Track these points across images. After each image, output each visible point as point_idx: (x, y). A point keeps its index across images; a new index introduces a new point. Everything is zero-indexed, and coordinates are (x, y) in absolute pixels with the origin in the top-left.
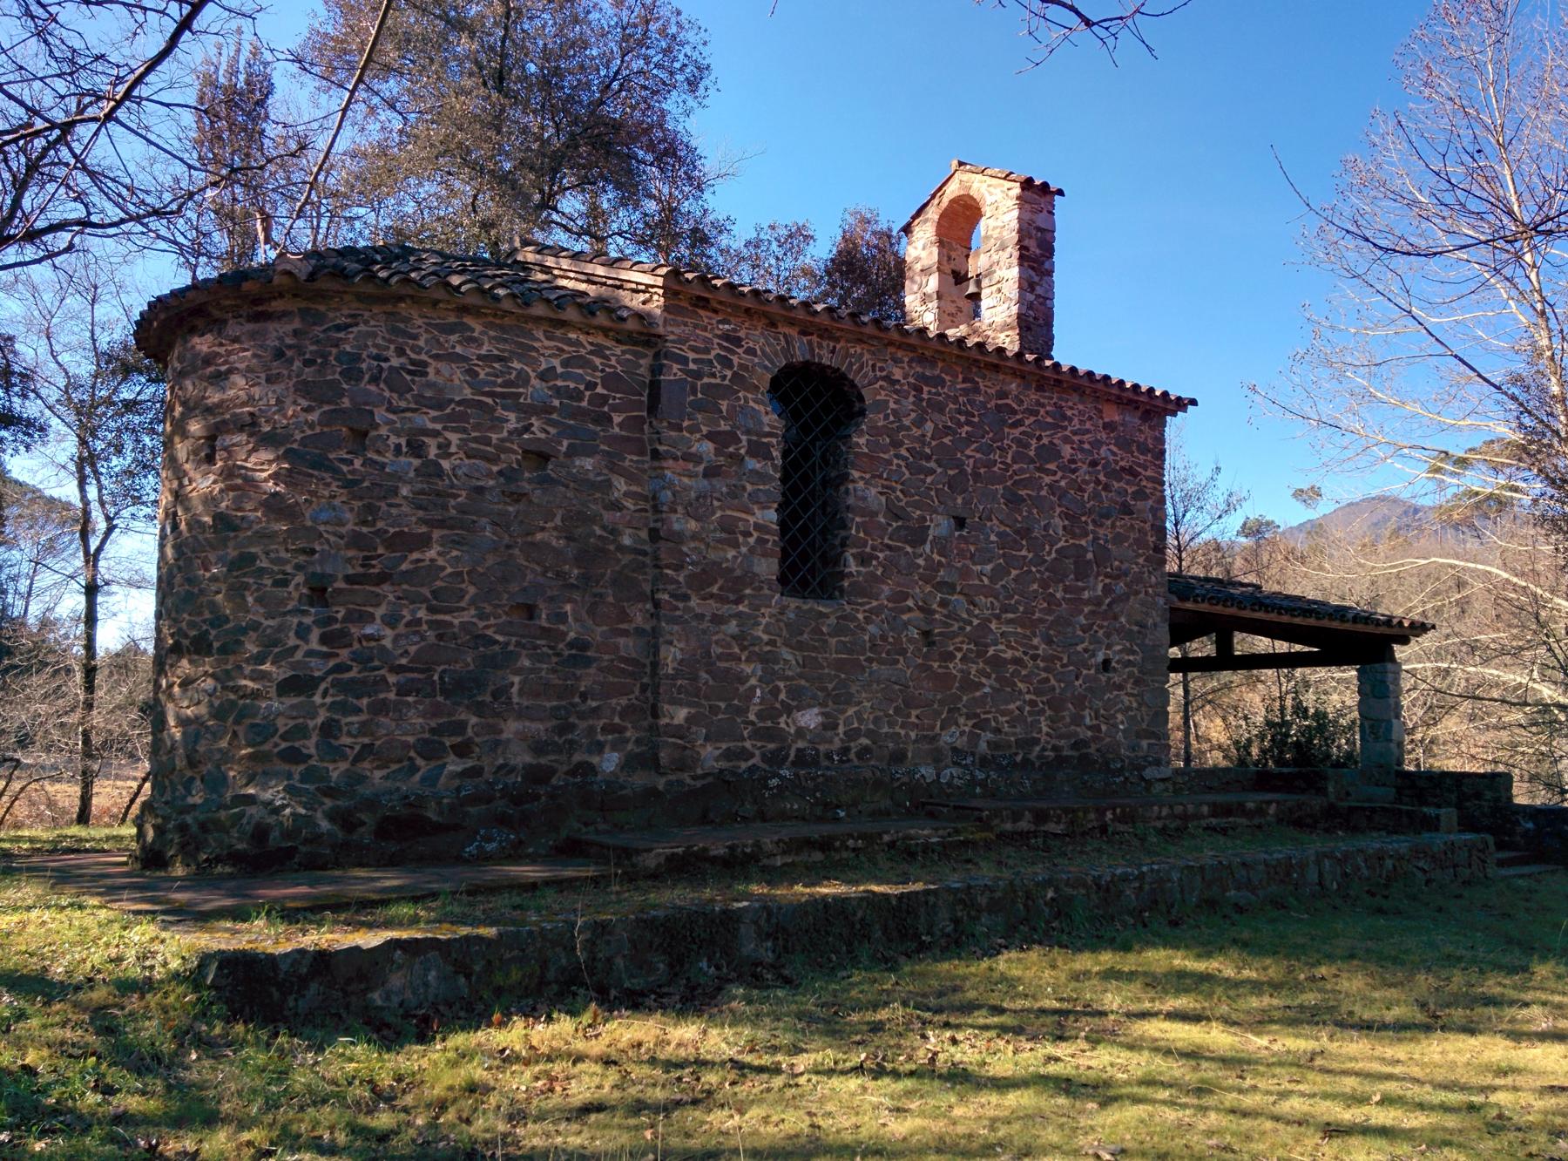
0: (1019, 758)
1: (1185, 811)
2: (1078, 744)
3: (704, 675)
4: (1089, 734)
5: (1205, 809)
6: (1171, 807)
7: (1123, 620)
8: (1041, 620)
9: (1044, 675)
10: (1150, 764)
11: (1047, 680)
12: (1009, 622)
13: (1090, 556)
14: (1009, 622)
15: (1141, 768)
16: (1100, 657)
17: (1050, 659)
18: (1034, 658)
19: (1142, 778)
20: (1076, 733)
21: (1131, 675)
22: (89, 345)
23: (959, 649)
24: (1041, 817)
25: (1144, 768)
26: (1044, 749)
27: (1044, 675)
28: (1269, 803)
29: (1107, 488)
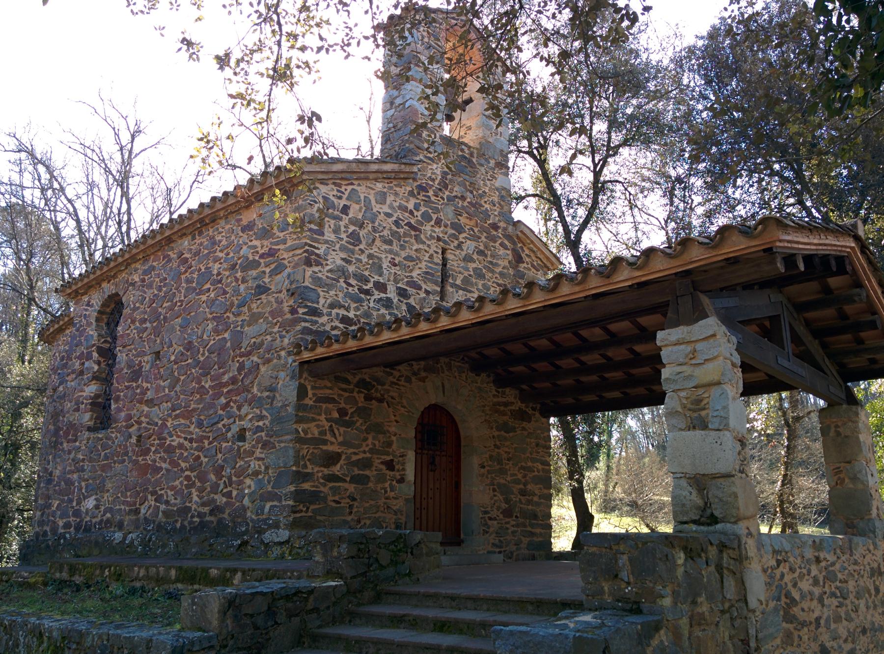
0: (178, 525)
1: (158, 573)
2: (216, 510)
3: (860, 138)
4: (224, 500)
5: (173, 573)
6: (147, 569)
7: (255, 390)
8: (194, 410)
9: (196, 453)
10: (270, 527)
11: (199, 457)
12: (177, 417)
13: (229, 344)
14: (177, 417)
15: (261, 532)
16: (235, 429)
17: (200, 440)
18: (191, 441)
19: (262, 542)
20: (214, 501)
21: (258, 441)
22: (85, 180)
23: (153, 445)
24: (73, 570)
25: (265, 531)
26: (192, 517)
27: (196, 453)
28: (234, 571)
29: (244, 281)
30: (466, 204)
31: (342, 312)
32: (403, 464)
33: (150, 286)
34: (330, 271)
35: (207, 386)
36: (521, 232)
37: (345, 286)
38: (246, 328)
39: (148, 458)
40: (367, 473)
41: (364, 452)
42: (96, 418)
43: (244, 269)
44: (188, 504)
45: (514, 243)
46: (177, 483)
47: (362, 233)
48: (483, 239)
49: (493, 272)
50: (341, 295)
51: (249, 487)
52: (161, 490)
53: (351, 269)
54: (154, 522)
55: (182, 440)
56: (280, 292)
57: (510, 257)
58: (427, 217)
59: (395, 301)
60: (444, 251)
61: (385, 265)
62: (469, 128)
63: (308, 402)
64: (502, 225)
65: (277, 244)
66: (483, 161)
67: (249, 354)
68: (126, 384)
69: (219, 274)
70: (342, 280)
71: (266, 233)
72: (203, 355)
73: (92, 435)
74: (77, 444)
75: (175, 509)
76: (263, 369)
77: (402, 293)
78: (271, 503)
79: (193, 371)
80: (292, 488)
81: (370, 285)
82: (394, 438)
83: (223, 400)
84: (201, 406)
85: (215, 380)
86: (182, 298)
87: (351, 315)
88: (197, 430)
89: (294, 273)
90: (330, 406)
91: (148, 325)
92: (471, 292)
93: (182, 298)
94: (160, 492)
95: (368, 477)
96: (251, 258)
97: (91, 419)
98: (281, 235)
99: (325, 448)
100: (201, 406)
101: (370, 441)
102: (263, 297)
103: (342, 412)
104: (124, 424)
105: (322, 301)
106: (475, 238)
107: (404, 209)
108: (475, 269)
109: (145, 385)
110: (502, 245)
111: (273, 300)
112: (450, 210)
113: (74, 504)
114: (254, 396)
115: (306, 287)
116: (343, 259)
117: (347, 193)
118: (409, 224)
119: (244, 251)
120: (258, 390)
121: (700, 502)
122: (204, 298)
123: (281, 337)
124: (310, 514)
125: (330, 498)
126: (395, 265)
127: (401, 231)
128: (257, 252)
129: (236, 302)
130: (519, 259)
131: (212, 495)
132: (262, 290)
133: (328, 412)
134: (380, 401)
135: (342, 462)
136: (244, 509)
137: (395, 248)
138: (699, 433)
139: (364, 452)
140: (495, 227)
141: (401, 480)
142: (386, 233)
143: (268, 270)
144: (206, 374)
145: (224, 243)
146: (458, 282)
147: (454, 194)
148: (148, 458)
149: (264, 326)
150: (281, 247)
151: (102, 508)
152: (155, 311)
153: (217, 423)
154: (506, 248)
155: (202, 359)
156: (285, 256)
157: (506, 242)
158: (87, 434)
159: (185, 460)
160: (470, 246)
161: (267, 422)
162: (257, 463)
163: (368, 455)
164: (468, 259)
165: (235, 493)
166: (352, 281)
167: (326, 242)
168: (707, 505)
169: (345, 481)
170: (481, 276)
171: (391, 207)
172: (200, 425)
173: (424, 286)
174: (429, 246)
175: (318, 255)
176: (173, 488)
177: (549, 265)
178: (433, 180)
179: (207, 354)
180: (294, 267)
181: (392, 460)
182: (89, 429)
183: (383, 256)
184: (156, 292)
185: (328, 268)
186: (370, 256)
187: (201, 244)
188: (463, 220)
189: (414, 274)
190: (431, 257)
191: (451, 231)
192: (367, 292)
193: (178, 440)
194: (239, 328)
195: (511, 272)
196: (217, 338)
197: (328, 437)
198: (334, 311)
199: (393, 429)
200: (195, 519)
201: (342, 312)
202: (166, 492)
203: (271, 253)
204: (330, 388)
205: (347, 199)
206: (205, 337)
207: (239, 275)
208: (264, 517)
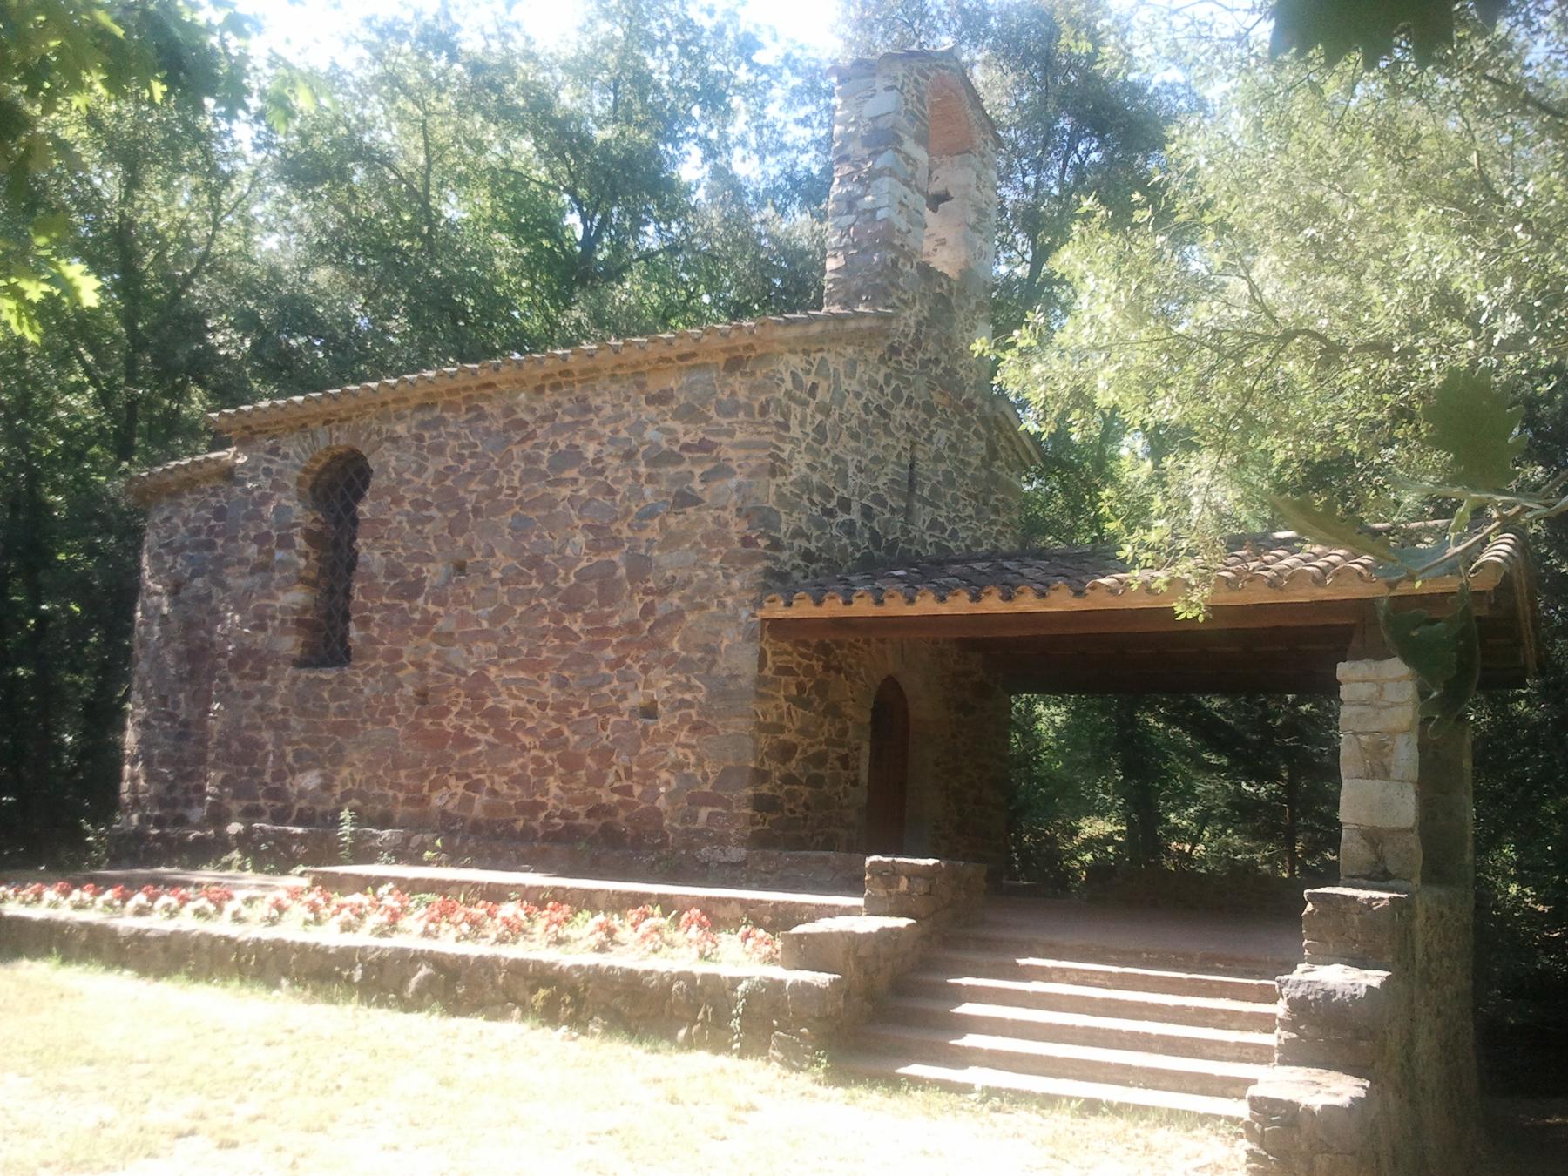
9: (555, 726)
13: (622, 572)
27: (555, 726)
29: (651, 479)
30: (940, 371)
31: (804, 543)
32: (858, 759)
33: (438, 450)
34: (793, 483)
35: (576, 628)
36: (1003, 413)
37: (807, 504)
38: (656, 553)
39: (444, 722)
40: (822, 772)
41: (820, 743)
42: (304, 645)
43: (653, 462)
44: (538, 798)
45: (989, 430)
46: (513, 764)
47: (829, 423)
48: (956, 426)
49: (964, 475)
50: (804, 518)
51: (668, 783)
52: (478, 772)
53: (816, 478)
54: (463, 819)
55: (521, 704)
56: (724, 508)
57: (984, 452)
58: (897, 395)
59: (859, 524)
60: (913, 444)
61: (851, 470)
62: (943, 242)
63: (768, 672)
64: (978, 401)
65: (718, 433)
66: (963, 302)
67: (663, 593)
68: (385, 600)
69: (597, 460)
70: (805, 497)
71: (690, 413)
72: (565, 580)
73: (304, 673)
74: (266, 683)
75: (512, 802)
76: (690, 618)
77: (867, 513)
78: (710, 809)
79: (544, 601)
80: (749, 792)
81: (834, 502)
82: (849, 723)
83: (609, 653)
84: (563, 657)
85: (592, 622)
86: (516, 483)
87: (813, 547)
88: (554, 691)
89: (750, 485)
90: (790, 679)
91: (433, 512)
92: (938, 507)
93: (516, 483)
94: (475, 777)
95: (822, 778)
96: (665, 446)
97: (295, 646)
98: (724, 422)
99: (782, 737)
100: (563, 657)
101: (825, 728)
102: (690, 510)
103: (801, 687)
104: (384, 664)
105: (783, 527)
106: (947, 424)
107: (873, 383)
108: (946, 472)
109: (432, 608)
110: (976, 433)
111: (710, 519)
112: (921, 383)
113: (267, 778)
114: (675, 656)
115: (770, 509)
116: (808, 465)
117: (815, 364)
118: (878, 408)
119: (650, 433)
120: (683, 648)
121: (1373, 858)
122: (566, 491)
123: (726, 576)
124: (767, 827)
125: (786, 806)
126: (861, 471)
127: (870, 418)
128: (677, 441)
129: (636, 510)
130: (993, 454)
131: (590, 789)
132: (685, 499)
133: (786, 687)
134: (839, 670)
135: (797, 756)
136: (659, 814)
137: (862, 445)
138: (1378, 783)
139: (820, 743)
140: (970, 405)
141: (855, 783)
142: (854, 422)
143: (698, 471)
144: (572, 610)
145: (608, 411)
146: (926, 493)
147: (928, 356)
148: (444, 722)
149: (693, 556)
150: (725, 440)
151: (338, 791)
152: (451, 492)
153: (601, 685)
154: (980, 439)
155: (563, 586)
156: (731, 453)
157: (982, 431)
158: (290, 671)
159: (531, 732)
160: (942, 435)
161: (700, 696)
162: (680, 750)
163: (824, 747)
164: (939, 458)
165: (637, 790)
166: (816, 498)
167: (792, 440)
168: (1381, 859)
169: (799, 783)
170: (951, 483)
171: (861, 383)
172: (561, 683)
173: (890, 502)
174: (898, 440)
175: (783, 461)
176: (505, 772)
177: (1027, 462)
178: (906, 336)
179: (573, 580)
180: (750, 476)
181: (847, 756)
182: (300, 664)
183: (849, 458)
184: (451, 463)
185: (792, 478)
186: (836, 459)
187: (557, 405)
188: (936, 397)
189: (880, 483)
190: (899, 456)
191: (923, 416)
192: (830, 513)
193: (512, 702)
194: (642, 551)
195: (984, 473)
196: (595, 559)
197: (786, 721)
198: (796, 543)
199: (849, 711)
200: (556, 821)
201: (804, 543)
202: (490, 778)
203: (704, 446)
204: (790, 654)
205: (817, 373)
206: (568, 552)
207: (643, 470)
208: (697, 826)
